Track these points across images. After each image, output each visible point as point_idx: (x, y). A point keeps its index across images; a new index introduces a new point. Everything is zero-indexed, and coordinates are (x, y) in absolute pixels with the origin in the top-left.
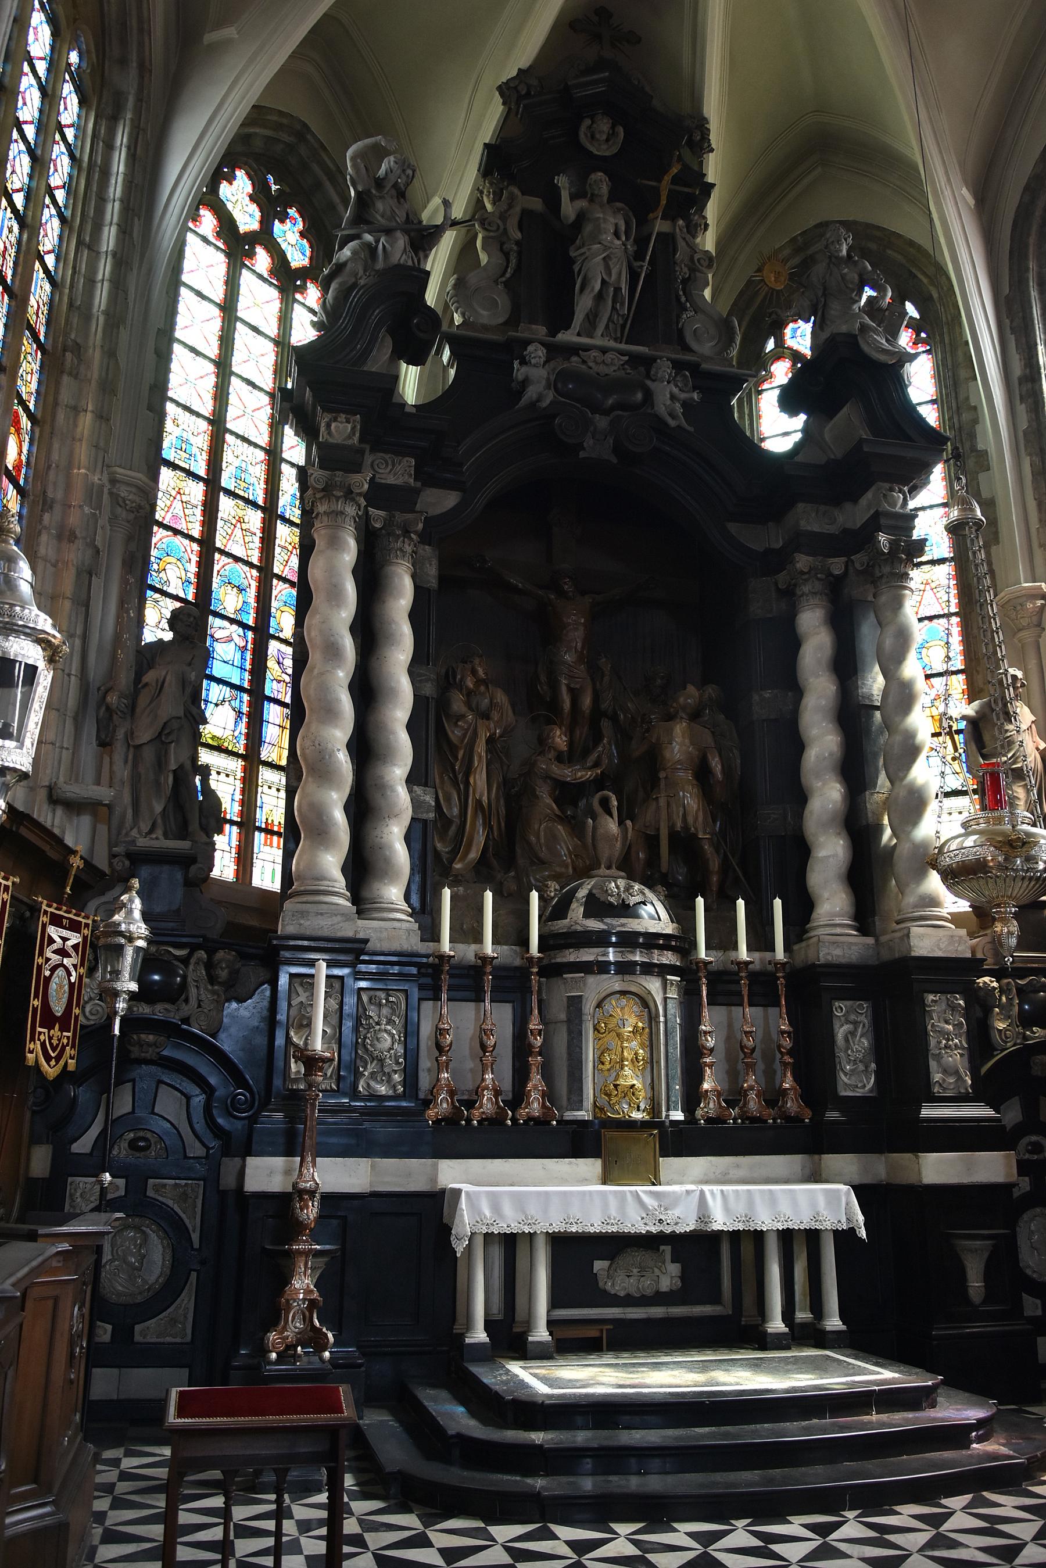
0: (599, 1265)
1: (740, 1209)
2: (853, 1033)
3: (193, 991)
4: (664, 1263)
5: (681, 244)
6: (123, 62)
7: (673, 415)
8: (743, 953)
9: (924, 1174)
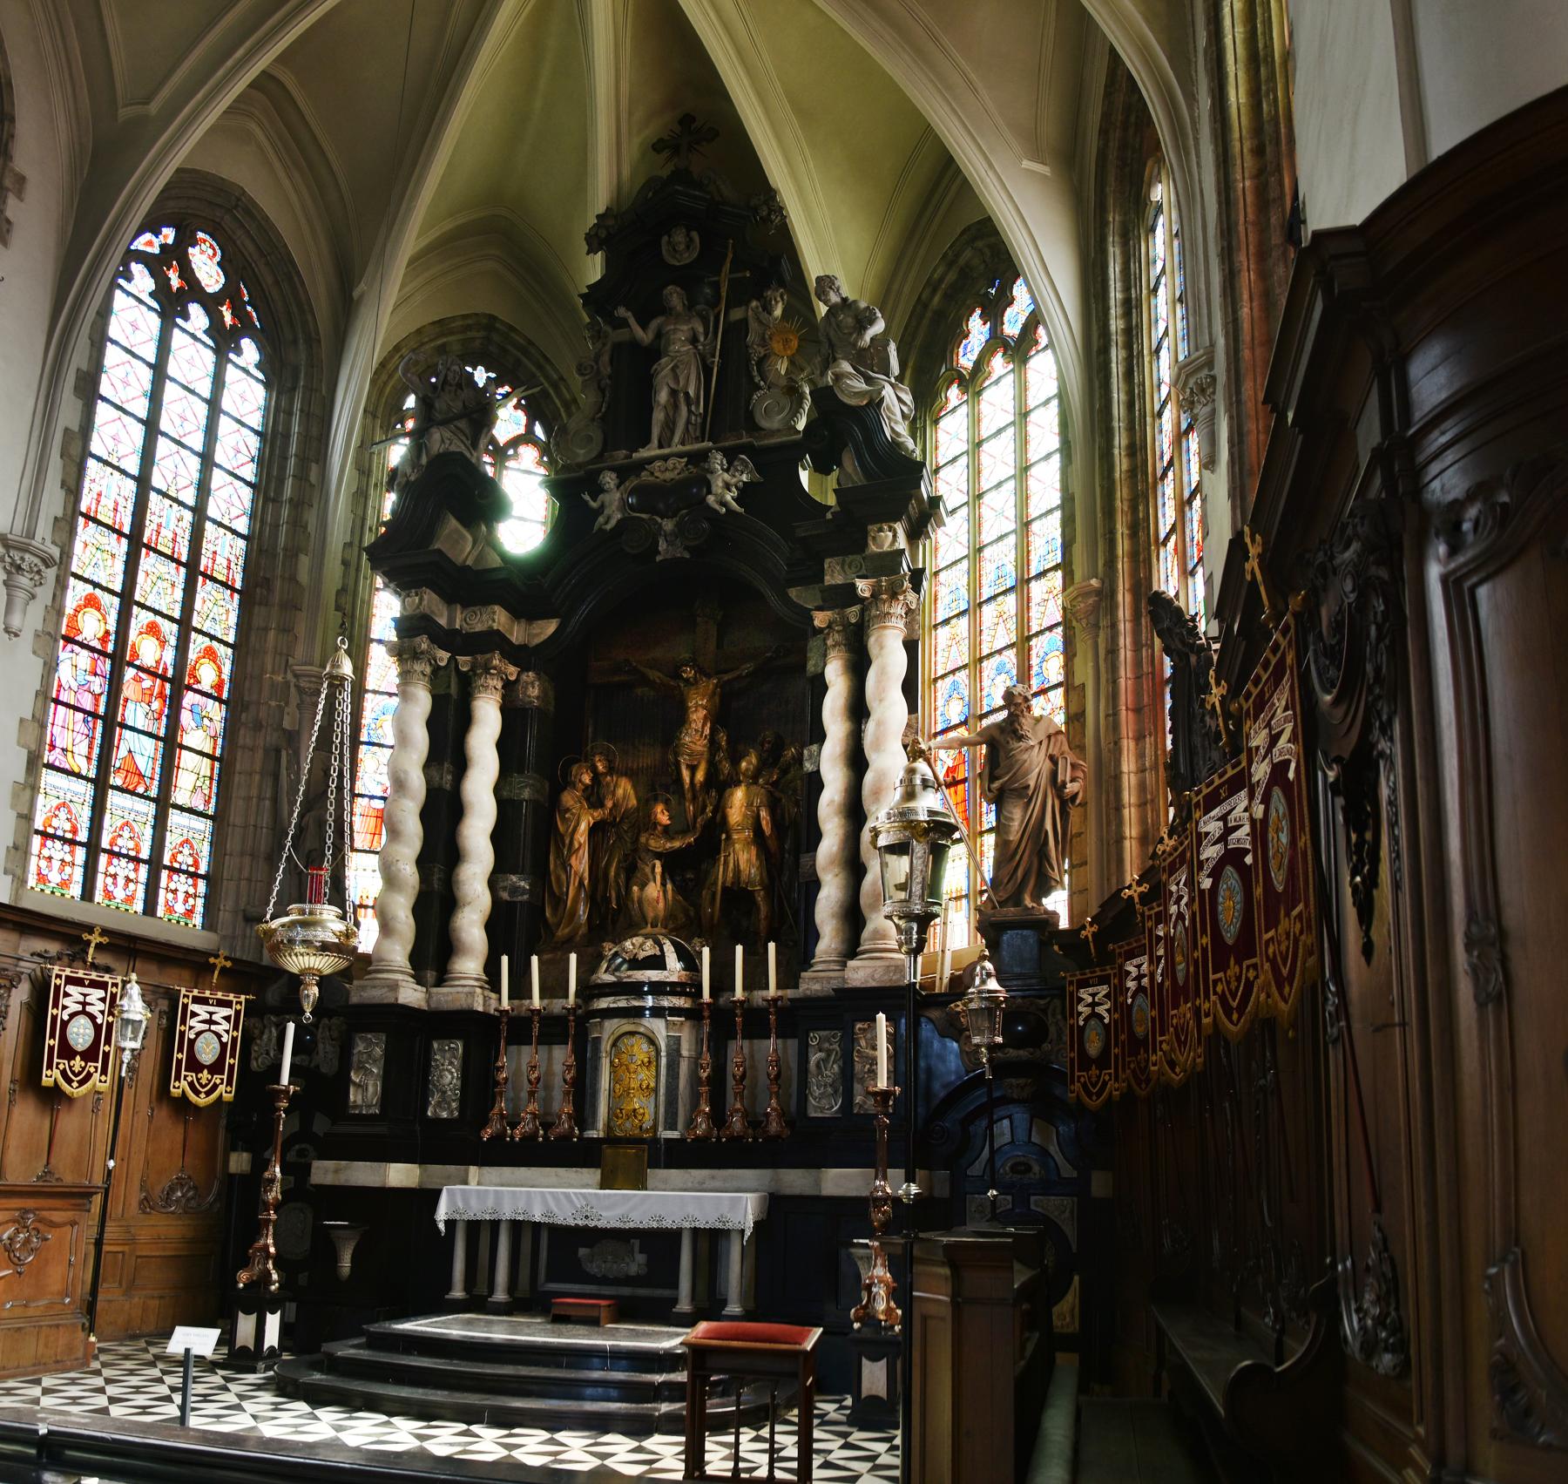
0: (582, 1252)
1: (490, 1203)
2: (825, 1060)
3: (321, 1046)
4: (632, 1252)
5: (753, 325)
6: (295, 342)
7: (724, 504)
8: (536, 1002)
9: (823, 1185)
